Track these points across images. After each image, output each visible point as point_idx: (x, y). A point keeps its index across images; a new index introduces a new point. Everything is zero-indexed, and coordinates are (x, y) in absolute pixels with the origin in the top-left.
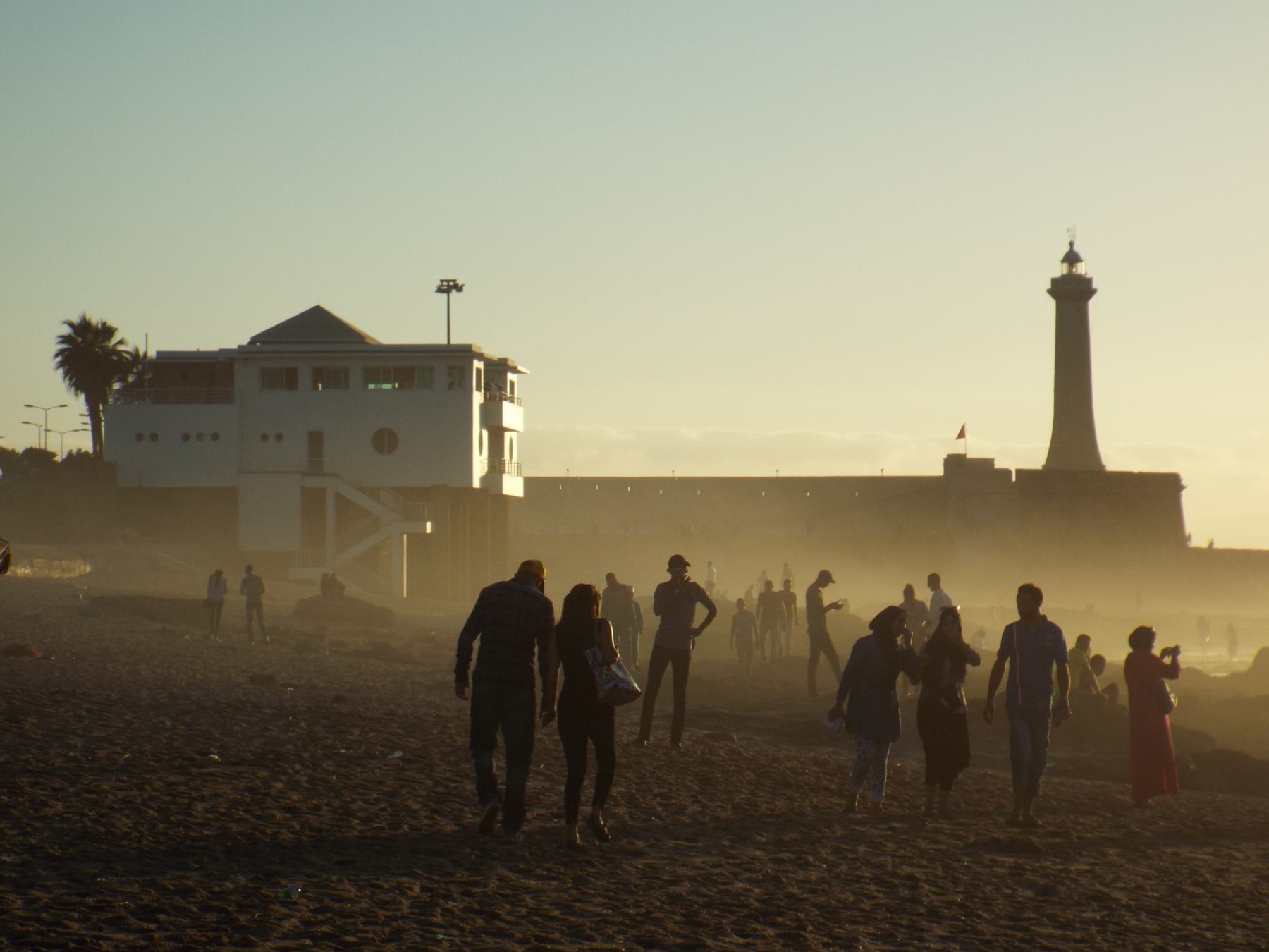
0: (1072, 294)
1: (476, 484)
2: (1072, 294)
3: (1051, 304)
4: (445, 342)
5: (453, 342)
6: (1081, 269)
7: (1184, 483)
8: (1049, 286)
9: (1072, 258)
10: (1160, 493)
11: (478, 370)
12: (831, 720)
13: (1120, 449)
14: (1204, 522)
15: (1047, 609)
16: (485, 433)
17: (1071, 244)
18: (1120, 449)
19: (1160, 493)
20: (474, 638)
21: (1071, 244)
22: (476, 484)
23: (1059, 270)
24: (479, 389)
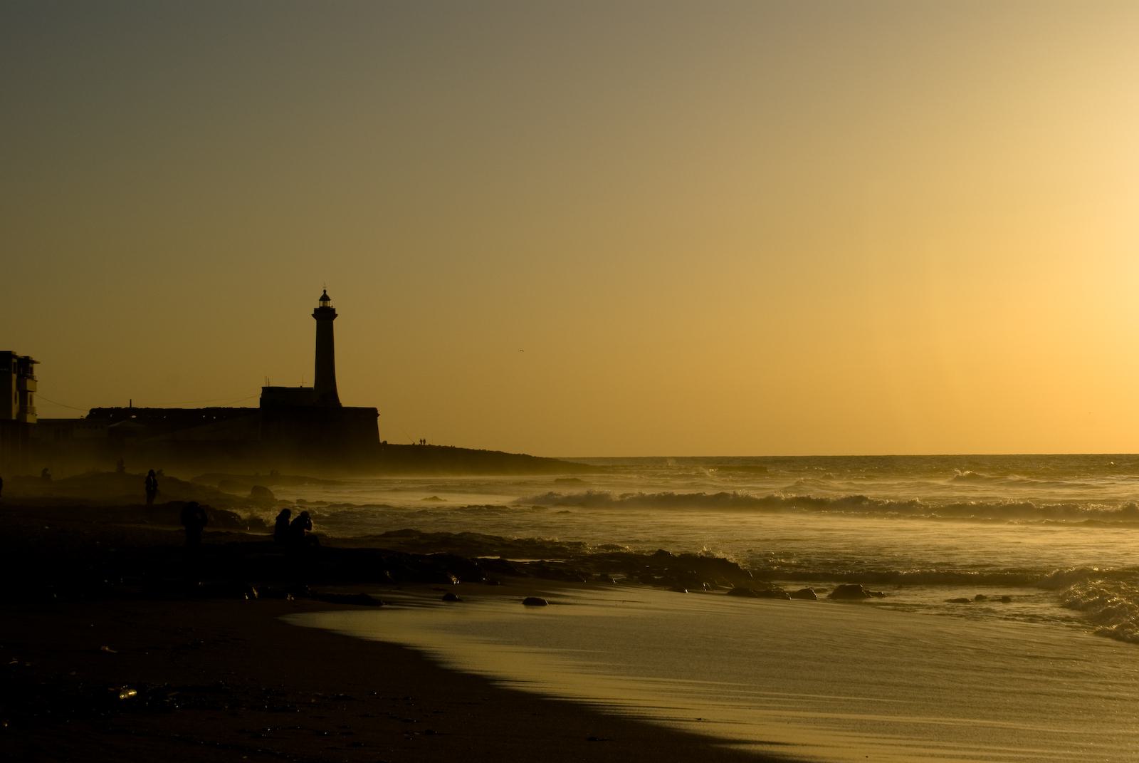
0: (325, 316)
1: (14, 417)
2: (325, 316)
3: (314, 321)
4: (129, 406)
5: (133, 406)
6: (331, 304)
7: (379, 412)
8: (313, 313)
9: (325, 298)
10: (368, 417)
11: (15, 363)
12: (297, 503)
13: (349, 395)
14: (391, 431)
15: (327, 293)
16: (18, 393)
17: (325, 291)
18: (349, 395)
19: (368, 417)
20: (969, 470)
21: (325, 291)
22: (14, 417)
23: (317, 305)
24: (15, 373)
